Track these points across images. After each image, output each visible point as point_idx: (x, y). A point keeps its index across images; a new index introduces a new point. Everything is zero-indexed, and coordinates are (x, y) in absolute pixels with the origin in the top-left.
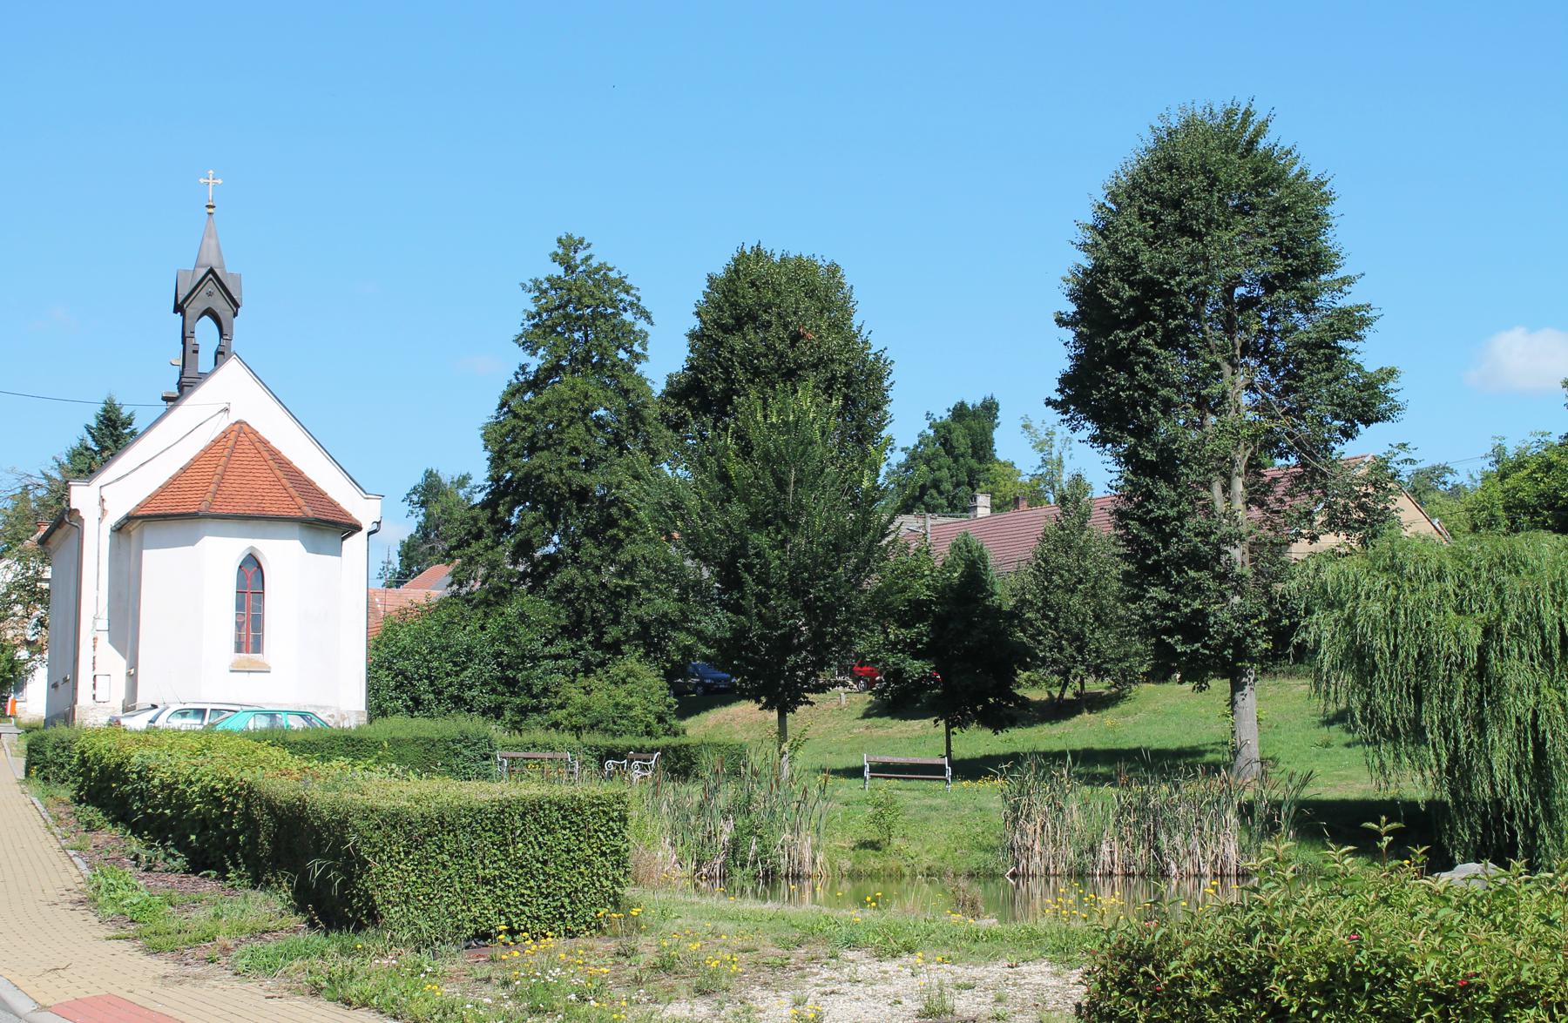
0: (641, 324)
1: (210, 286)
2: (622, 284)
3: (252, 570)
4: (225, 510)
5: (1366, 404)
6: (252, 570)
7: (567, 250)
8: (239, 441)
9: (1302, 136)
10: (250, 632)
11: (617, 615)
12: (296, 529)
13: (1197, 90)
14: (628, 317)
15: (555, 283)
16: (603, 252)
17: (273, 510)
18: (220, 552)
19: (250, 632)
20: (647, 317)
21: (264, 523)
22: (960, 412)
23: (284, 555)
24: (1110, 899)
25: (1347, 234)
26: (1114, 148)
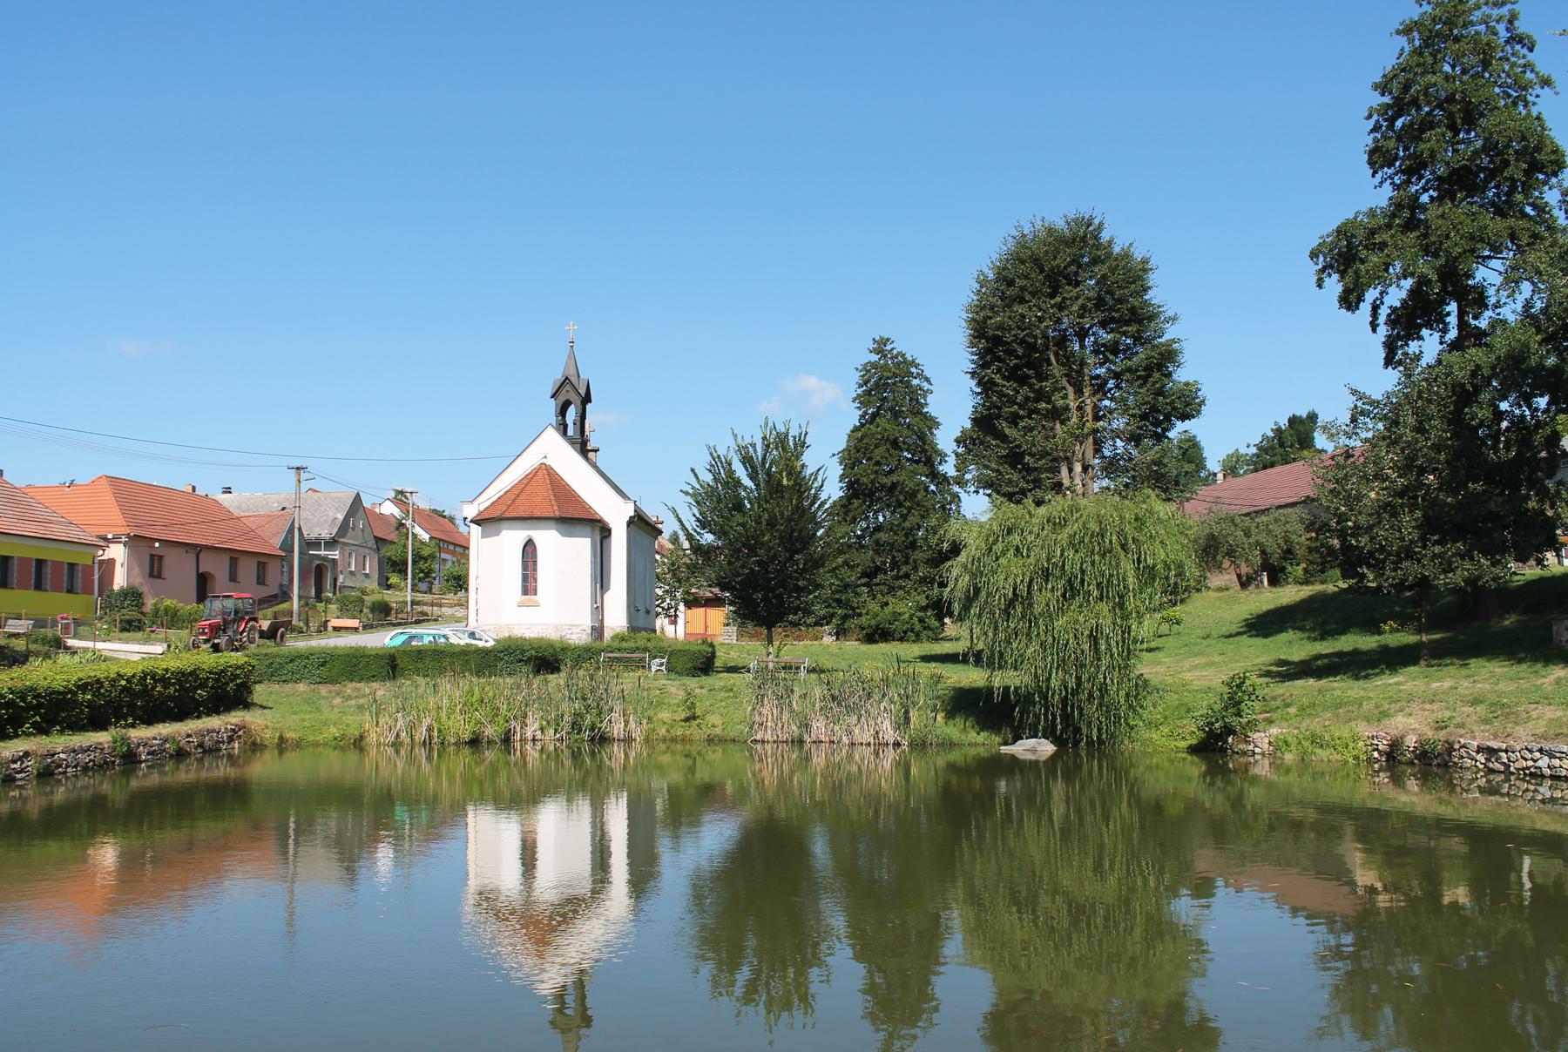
0: (926, 386)
1: (568, 387)
2: (913, 363)
3: (529, 548)
4: (514, 514)
5: (1188, 405)
6: (529, 548)
7: (881, 346)
8: (546, 475)
9: (1122, 233)
10: (529, 585)
11: (907, 558)
12: (553, 524)
13: (1052, 209)
14: (915, 382)
15: (874, 365)
16: (901, 345)
17: (538, 514)
18: (512, 539)
19: (529, 585)
20: (928, 380)
21: (516, 524)
22: (1293, 421)
23: (548, 540)
24: (867, 737)
25: (1161, 292)
26: (982, 251)
